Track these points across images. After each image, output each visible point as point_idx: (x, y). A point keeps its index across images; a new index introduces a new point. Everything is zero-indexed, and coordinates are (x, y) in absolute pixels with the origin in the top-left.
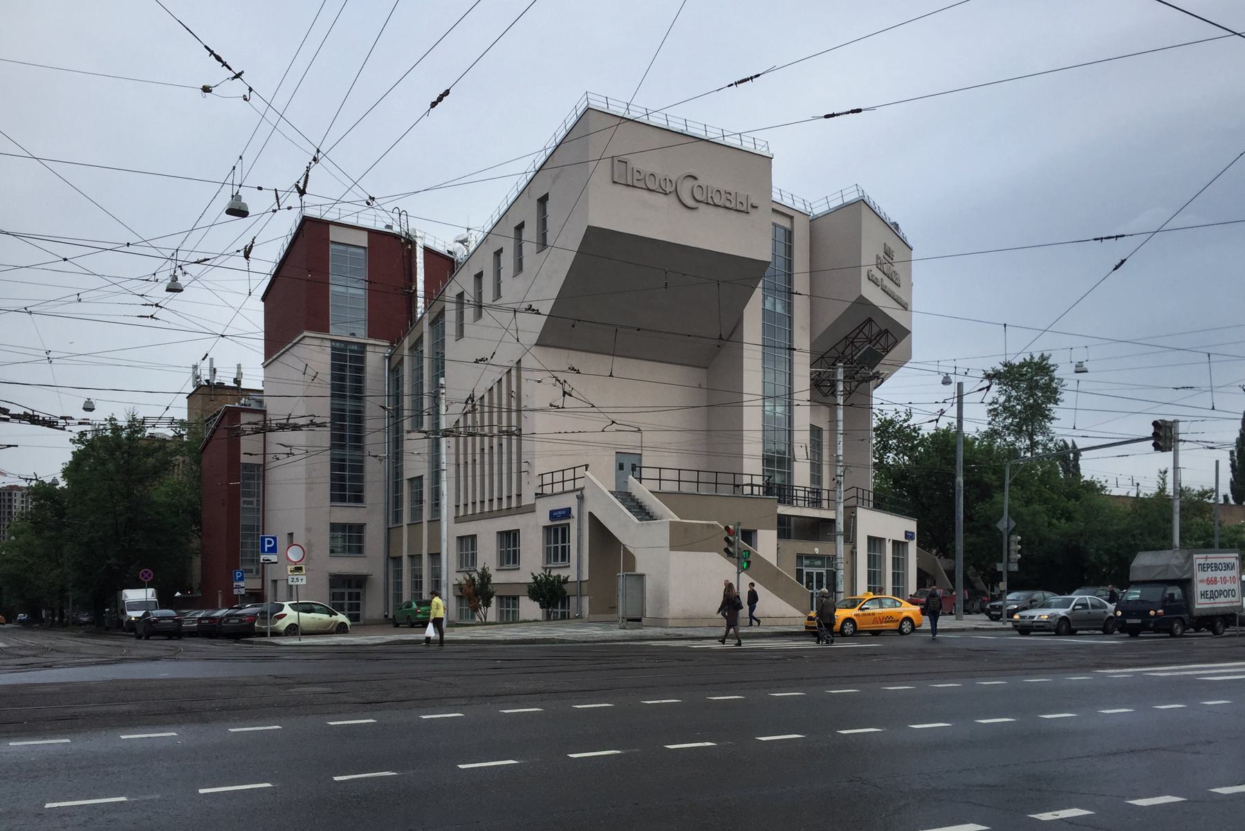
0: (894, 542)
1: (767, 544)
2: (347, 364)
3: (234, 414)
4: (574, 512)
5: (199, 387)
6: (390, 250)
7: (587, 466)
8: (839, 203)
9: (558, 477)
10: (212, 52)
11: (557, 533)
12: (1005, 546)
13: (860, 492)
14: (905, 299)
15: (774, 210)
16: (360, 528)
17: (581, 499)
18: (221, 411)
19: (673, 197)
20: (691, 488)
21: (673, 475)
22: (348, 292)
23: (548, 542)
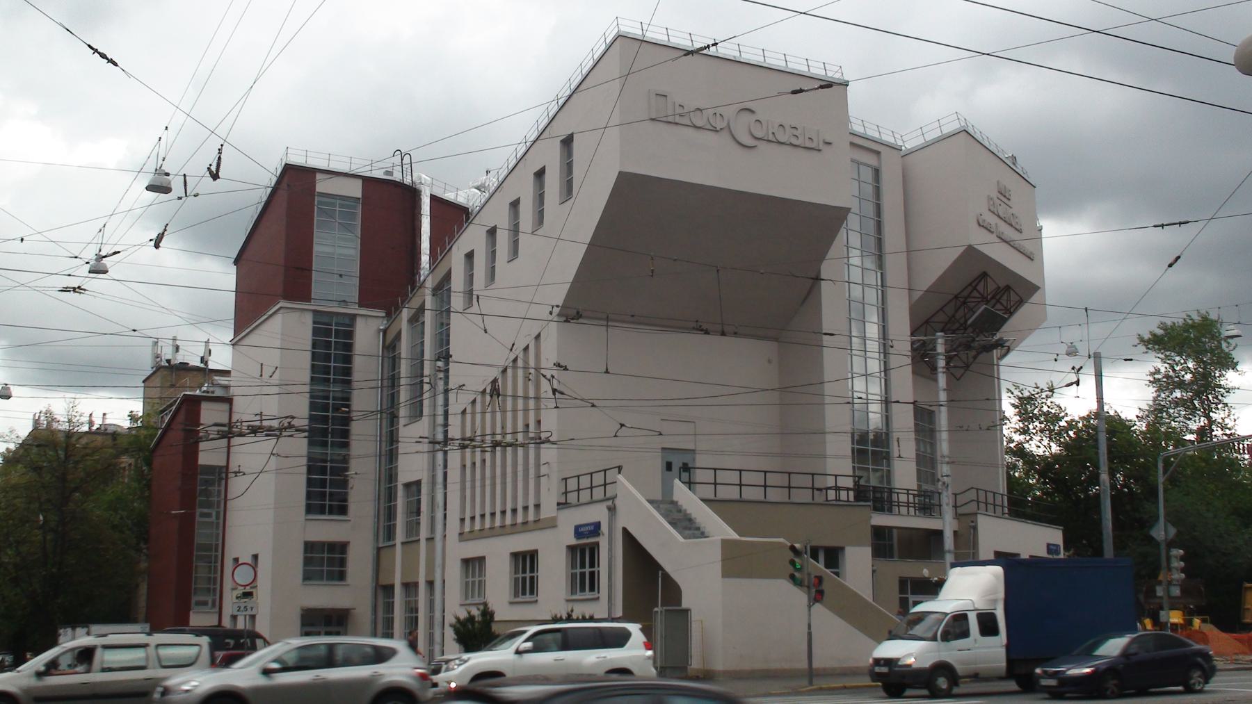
1: (858, 564)
2: (331, 350)
3: (192, 404)
4: (604, 528)
5: (158, 369)
6: (389, 204)
7: (620, 468)
8: (936, 134)
9: (585, 482)
10: (96, 51)
11: (583, 554)
13: (982, 494)
15: (852, 144)
17: (612, 510)
18: (183, 396)
19: (725, 134)
21: (734, 477)
22: (337, 251)
23: (573, 566)
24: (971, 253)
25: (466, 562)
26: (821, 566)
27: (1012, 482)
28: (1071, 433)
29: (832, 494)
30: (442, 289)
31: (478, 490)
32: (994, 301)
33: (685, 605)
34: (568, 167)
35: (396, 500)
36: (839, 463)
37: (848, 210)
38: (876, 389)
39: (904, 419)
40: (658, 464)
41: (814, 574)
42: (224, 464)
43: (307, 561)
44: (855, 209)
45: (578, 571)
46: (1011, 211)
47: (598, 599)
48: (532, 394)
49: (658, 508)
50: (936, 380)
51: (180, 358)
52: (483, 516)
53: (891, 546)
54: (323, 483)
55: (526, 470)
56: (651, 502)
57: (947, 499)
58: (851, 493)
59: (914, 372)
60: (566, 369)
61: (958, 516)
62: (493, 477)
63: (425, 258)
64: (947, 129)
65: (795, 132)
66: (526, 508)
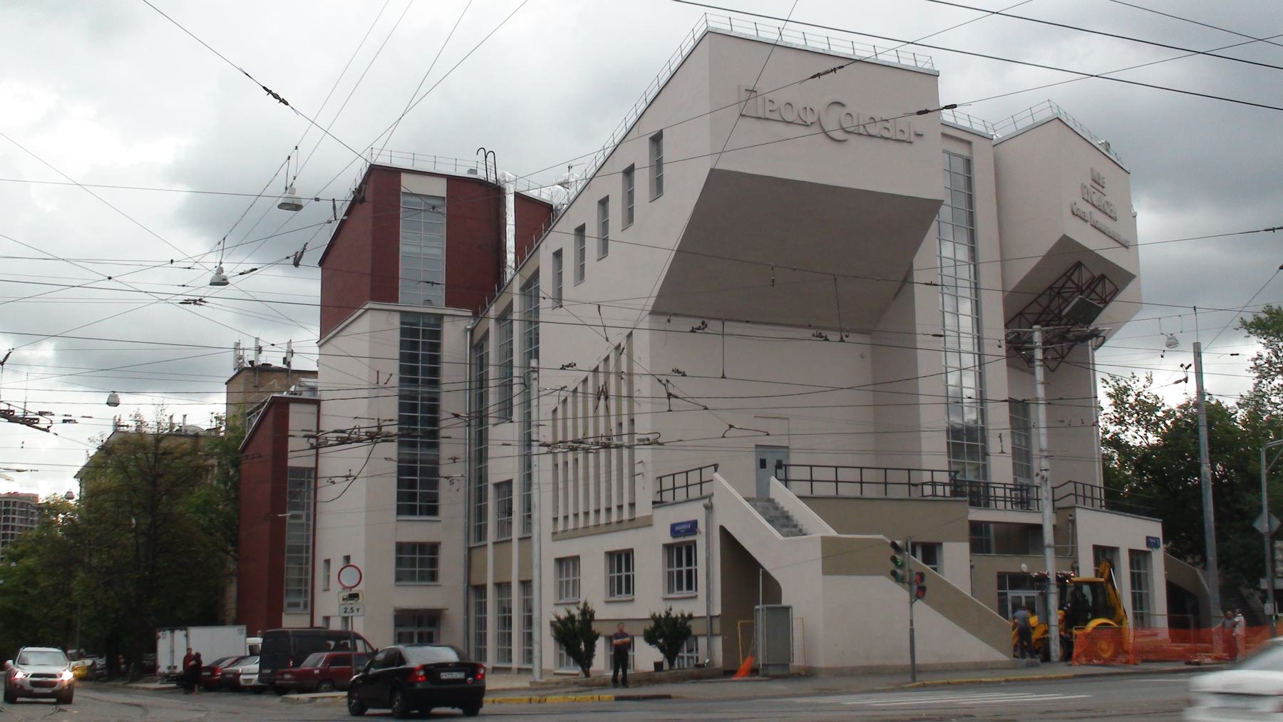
0: (1133, 552)
1: (956, 560)
2: (419, 347)
3: (279, 408)
4: (701, 526)
5: (241, 370)
6: (474, 201)
7: (716, 467)
8: (1029, 122)
9: (680, 480)
10: (270, 92)
11: (680, 553)
12: (1268, 557)
13: (1080, 487)
14: (1124, 236)
15: (944, 135)
16: (433, 548)
17: (709, 508)
18: (269, 397)
20: (853, 490)
21: (830, 474)
22: (423, 248)
23: (670, 564)
24: (1066, 243)
25: (560, 562)
26: (919, 560)
27: (1107, 471)
28: (1168, 422)
29: (928, 490)
30: (531, 286)
31: (571, 490)
32: (1088, 291)
33: (785, 602)
34: (658, 165)
35: (486, 499)
36: (934, 457)
37: (941, 202)
38: (969, 381)
39: (999, 417)
40: (752, 462)
41: (916, 570)
42: (313, 465)
43: (399, 562)
44: (948, 201)
45: (675, 569)
46: (1106, 199)
47: (696, 597)
48: (624, 393)
49: (754, 506)
50: (1033, 374)
51: (263, 359)
52: (576, 515)
53: (988, 541)
54: (412, 484)
55: (620, 470)
56: (748, 500)
57: (1045, 493)
58: (947, 488)
59: (1009, 365)
60: (684, 375)
61: (1056, 510)
62: (586, 478)
63: (510, 257)
64: (1040, 117)
65: (886, 125)
66: (620, 507)
